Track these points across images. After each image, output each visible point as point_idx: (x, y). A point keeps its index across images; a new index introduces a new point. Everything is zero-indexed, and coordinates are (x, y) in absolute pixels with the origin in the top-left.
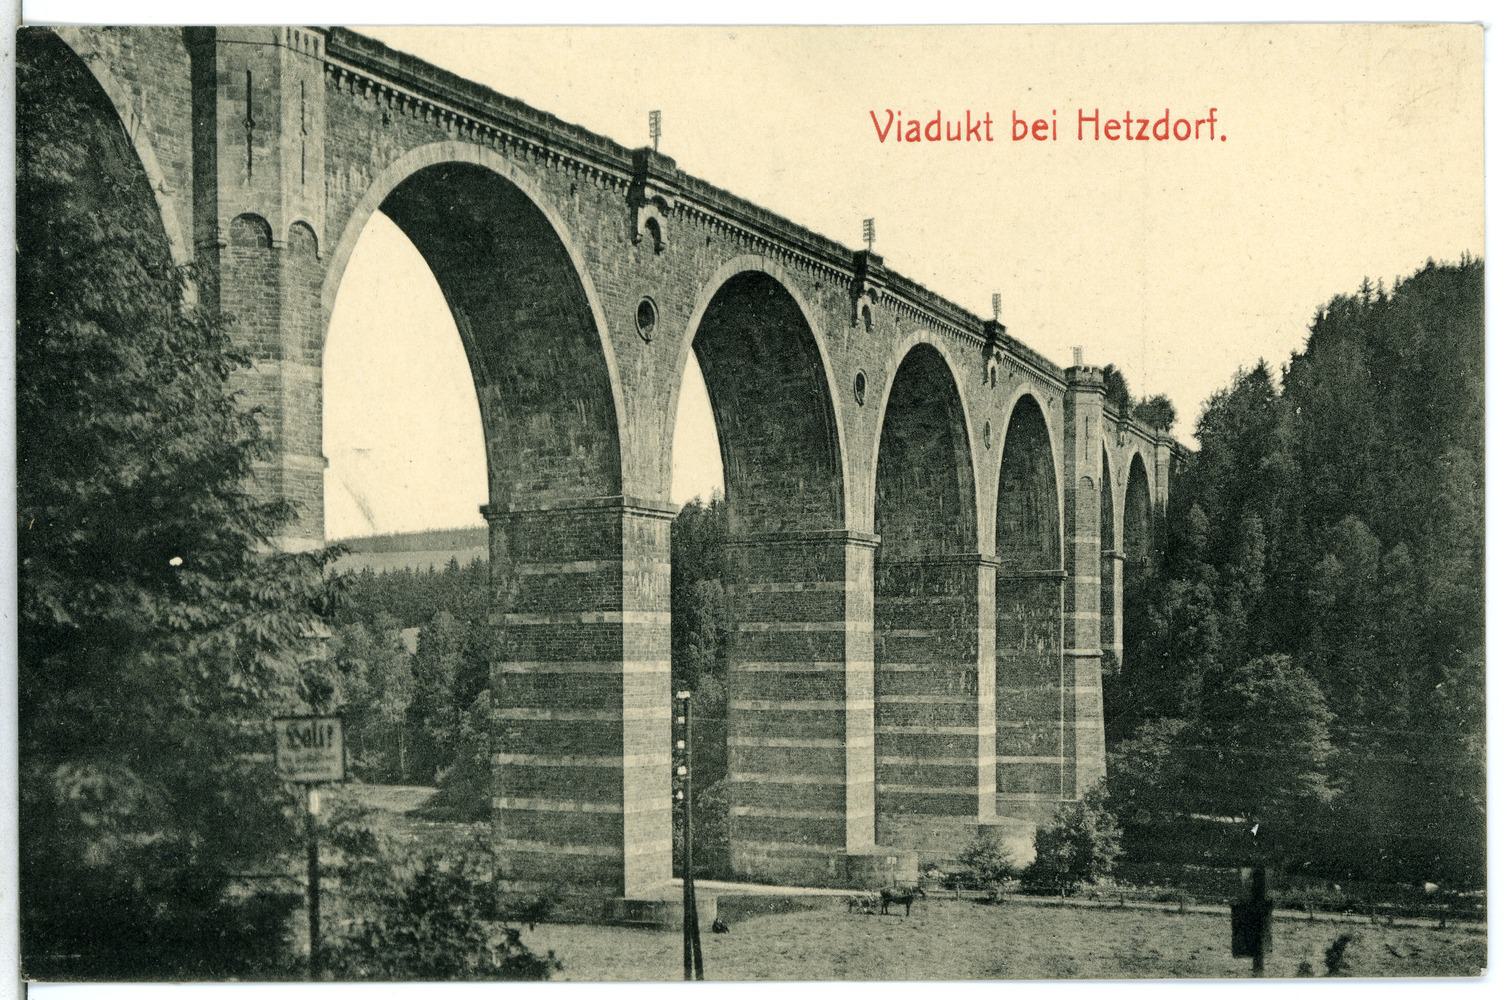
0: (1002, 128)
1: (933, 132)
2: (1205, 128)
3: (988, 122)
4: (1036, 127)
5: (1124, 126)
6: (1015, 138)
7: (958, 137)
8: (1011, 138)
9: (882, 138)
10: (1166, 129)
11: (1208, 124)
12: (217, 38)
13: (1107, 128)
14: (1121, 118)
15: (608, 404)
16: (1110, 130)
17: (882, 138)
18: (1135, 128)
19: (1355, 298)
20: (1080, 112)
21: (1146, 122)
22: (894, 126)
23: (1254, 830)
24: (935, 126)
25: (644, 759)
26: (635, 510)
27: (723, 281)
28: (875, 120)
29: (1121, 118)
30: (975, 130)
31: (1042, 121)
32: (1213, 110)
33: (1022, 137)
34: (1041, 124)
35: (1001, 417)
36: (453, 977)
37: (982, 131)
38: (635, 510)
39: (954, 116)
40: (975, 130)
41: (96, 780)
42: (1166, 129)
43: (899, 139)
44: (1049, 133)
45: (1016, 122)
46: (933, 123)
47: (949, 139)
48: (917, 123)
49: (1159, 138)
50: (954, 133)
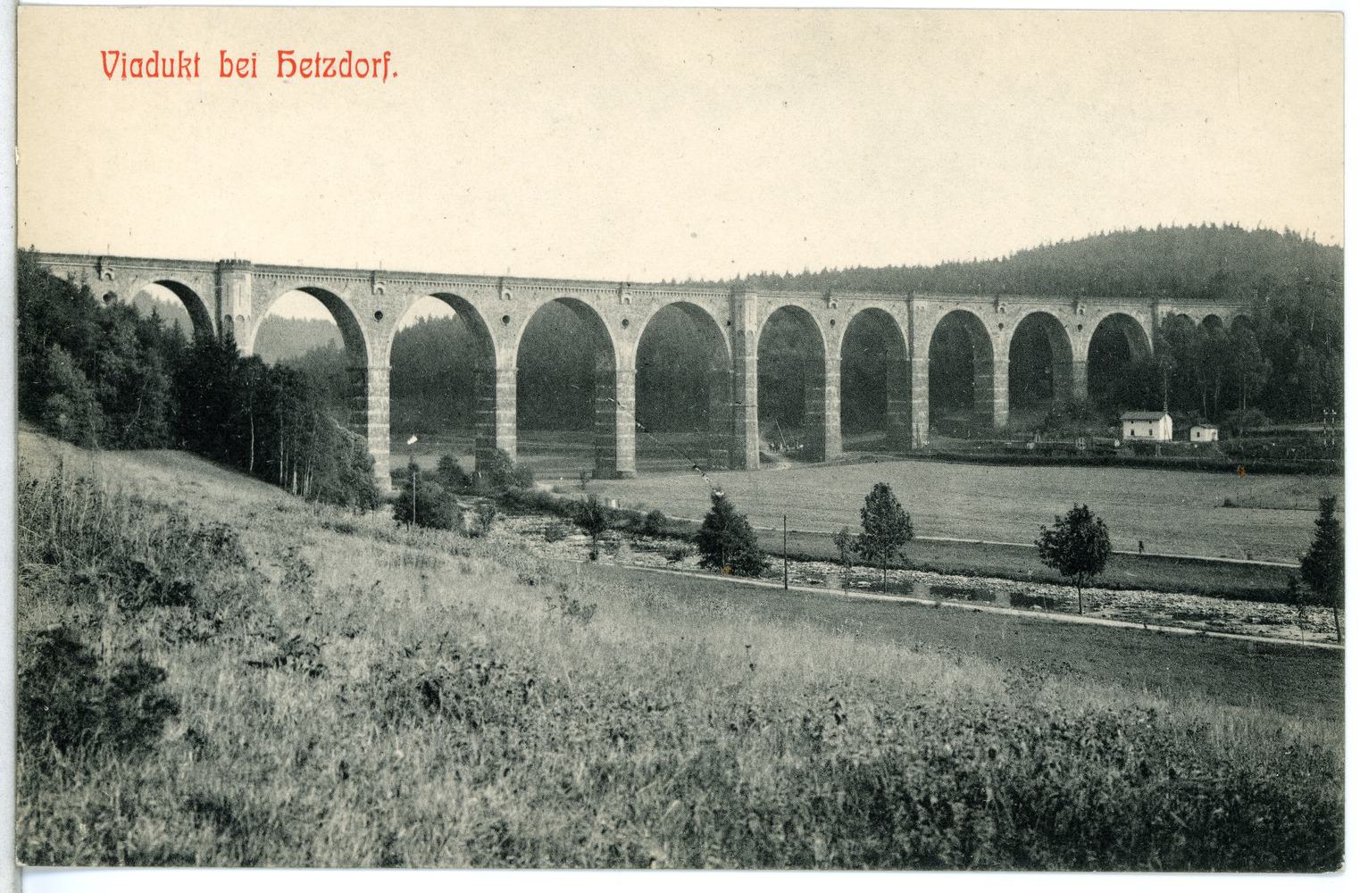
0: (210, 66)
3: (197, 59)
5: (314, 64)
6: (222, 74)
7: (172, 75)
8: (219, 73)
10: (348, 66)
12: (1074, 359)
15: (1296, 655)
17: (109, 75)
18: (323, 67)
22: (120, 63)
23: (414, 439)
24: (244, 63)
26: (1232, 728)
27: (1088, 345)
32: (388, 53)
33: (229, 75)
35: (827, 336)
37: (192, 68)
38: (1232, 728)
39: (168, 53)
40: (186, 67)
42: (348, 66)
43: (124, 75)
44: (250, 68)
47: (165, 75)
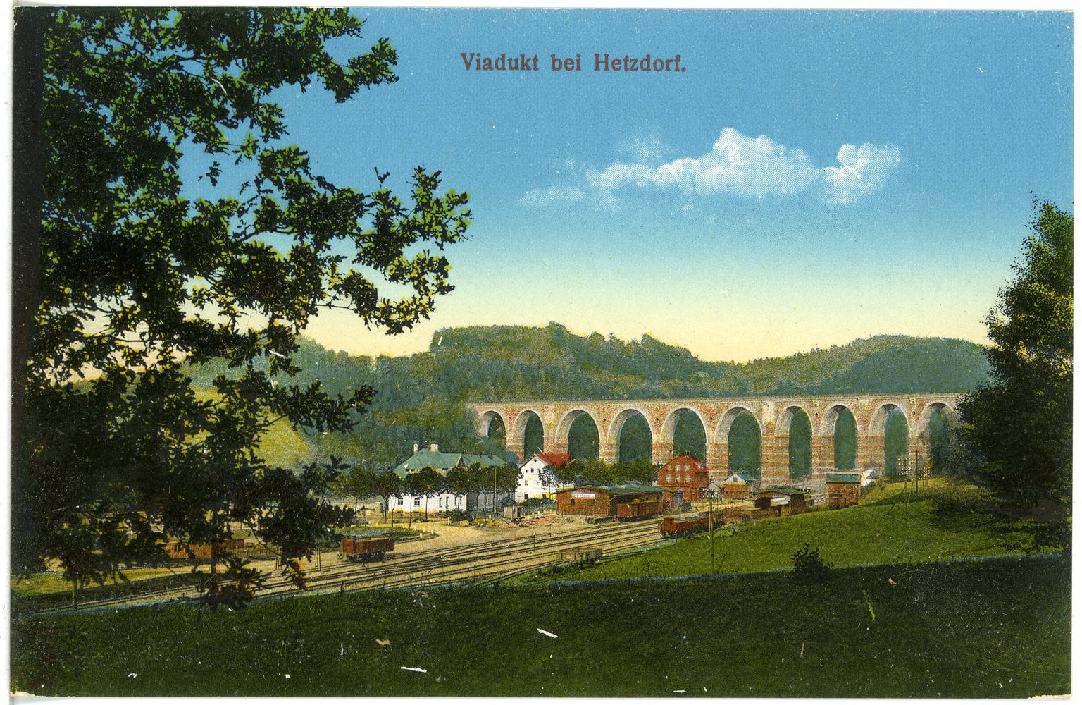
1: (500, 65)
2: (672, 65)
4: (566, 63)
6: (554, 68)
9: (468, 66)
11: (674, 63)
13: (613, 63)
14: (622, 58)
16: (488, 65)
17: (468, 66)
18: (629, 65)
19: (101, 379)
20: (553, 56)
21: (636, 61)
25: (766, 479)
28: (647, 64)
29: (622, 58)
30: (524, 64)
31: (617, 59)
34: (616, 62)
36: (1069, 519)
40: (524, 64)
41: (74, 378)
45: (554, 61)
46: (499, 59)
48: (490, 60)
49: (498, 69)
50: (513, 65)
